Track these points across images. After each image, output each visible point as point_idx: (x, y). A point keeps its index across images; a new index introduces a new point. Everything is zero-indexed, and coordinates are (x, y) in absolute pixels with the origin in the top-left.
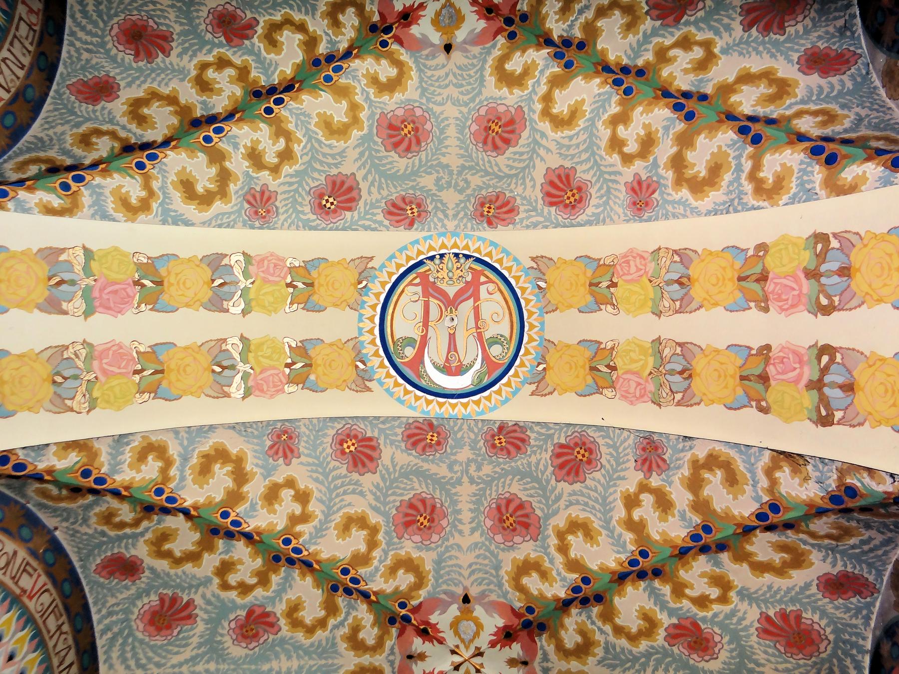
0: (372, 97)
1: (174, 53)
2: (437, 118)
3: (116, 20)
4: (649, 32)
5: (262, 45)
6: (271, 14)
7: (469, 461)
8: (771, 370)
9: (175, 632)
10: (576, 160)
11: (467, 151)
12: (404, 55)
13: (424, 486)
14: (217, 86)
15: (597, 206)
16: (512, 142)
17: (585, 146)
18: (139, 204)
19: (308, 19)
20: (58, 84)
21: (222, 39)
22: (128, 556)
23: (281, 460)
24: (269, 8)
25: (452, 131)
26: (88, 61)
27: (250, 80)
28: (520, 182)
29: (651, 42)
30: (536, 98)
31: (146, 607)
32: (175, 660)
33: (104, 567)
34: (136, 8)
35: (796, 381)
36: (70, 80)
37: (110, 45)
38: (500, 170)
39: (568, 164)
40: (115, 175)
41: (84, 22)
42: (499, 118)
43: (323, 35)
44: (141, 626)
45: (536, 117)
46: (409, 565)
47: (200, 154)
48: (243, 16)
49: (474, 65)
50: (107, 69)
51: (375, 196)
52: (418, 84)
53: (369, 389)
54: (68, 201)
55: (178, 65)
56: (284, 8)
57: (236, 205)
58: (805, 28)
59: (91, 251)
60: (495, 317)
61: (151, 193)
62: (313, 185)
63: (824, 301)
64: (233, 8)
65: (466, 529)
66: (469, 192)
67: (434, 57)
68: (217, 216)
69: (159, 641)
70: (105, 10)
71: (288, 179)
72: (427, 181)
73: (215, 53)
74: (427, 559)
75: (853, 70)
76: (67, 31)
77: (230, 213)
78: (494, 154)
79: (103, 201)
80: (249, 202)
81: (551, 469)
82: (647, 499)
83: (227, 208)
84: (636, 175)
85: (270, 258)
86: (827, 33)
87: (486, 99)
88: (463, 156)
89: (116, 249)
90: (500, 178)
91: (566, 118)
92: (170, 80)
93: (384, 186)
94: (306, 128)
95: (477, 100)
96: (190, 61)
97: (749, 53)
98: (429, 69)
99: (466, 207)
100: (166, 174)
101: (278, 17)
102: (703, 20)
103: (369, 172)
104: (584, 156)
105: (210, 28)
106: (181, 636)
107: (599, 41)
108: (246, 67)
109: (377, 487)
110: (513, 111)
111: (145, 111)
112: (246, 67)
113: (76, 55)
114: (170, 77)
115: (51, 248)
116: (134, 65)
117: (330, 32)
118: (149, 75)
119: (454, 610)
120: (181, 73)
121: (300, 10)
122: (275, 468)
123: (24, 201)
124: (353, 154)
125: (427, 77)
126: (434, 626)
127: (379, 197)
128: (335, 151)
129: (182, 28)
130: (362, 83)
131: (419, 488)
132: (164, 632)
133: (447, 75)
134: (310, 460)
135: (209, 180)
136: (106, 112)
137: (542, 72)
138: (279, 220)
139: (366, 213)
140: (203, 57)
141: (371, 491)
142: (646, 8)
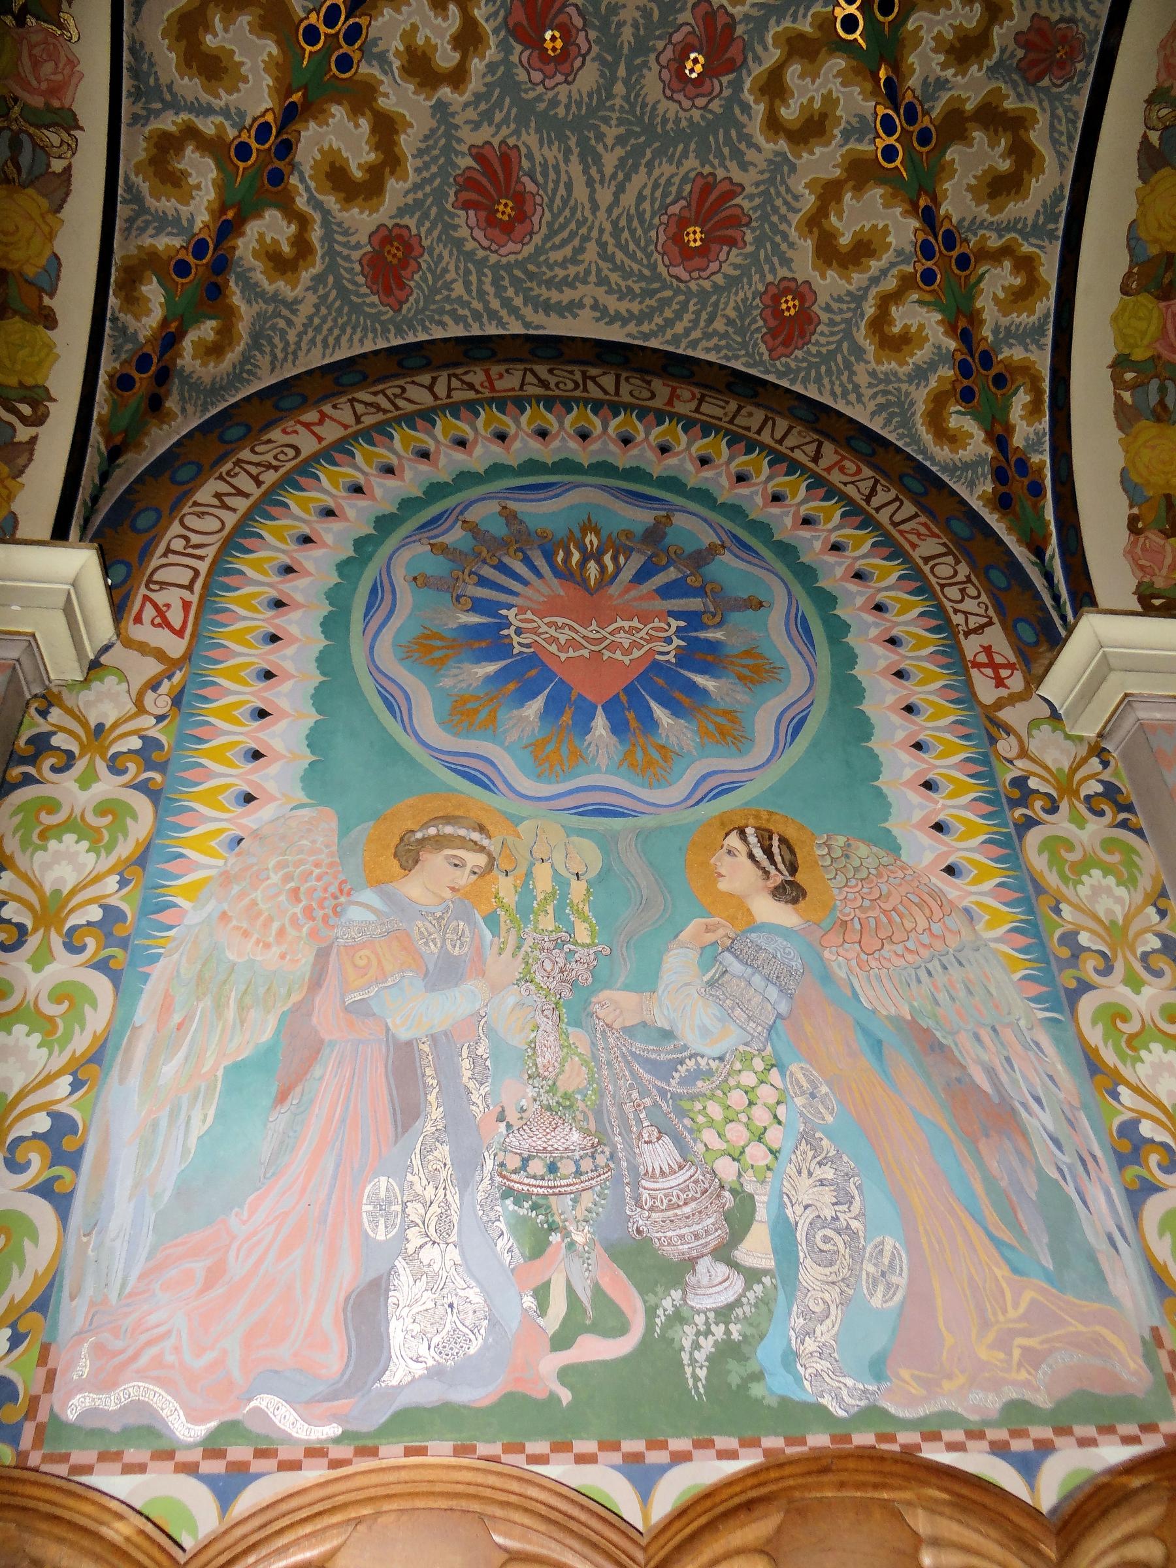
1: (737, 175)
3: (661, 269)
9: (530, 187)
14: (817, 105)
18: (1023, 273)
20: (768, 372)
21: (725, 80)
22: (368, 248)
26: (730, 322)
27: (818, 35)
31: (478, 234)
32: (581, 193)
33: (388, 291)
34: (646, 232)
36: (761, 355)
37: (707, 285)
40: (978, 304)
41: (658, 320)
44: (511, 246)
47: (948, 157)
48: (687, 29)
50: (750, 295)
54: (1020, 380)
55: (762, 172)
57: (1041, 102)
59: (1118, 356)
61: (1006, 251)
64: (670, 47)
69: (541, 220)
73: (750, 99)
76: (670, 348)
77: (1054, 116)
79: (1018, 327)
80: (1040, 77)
83: (1043, 120)
85: (1168, 52)
89: (1115, 319)
92: (788, 190)
96: (759, 150)
100: (978, 221)
105: (701, 102)
106: (540, 179)
108: (789, 41)
111: (845, 240)
112: (789, 41)
113: (715, 340)
114: (782, 189)
115: (1116, 413)
116: (749, 249)
118: (773, 226)
120: (779, 167)
123: (1027, 439)
129: (692, 155)
132: (528, 208)
135: (992, 146)
136: (835, 306)
138: (1083, 20)
140: (755, 126)
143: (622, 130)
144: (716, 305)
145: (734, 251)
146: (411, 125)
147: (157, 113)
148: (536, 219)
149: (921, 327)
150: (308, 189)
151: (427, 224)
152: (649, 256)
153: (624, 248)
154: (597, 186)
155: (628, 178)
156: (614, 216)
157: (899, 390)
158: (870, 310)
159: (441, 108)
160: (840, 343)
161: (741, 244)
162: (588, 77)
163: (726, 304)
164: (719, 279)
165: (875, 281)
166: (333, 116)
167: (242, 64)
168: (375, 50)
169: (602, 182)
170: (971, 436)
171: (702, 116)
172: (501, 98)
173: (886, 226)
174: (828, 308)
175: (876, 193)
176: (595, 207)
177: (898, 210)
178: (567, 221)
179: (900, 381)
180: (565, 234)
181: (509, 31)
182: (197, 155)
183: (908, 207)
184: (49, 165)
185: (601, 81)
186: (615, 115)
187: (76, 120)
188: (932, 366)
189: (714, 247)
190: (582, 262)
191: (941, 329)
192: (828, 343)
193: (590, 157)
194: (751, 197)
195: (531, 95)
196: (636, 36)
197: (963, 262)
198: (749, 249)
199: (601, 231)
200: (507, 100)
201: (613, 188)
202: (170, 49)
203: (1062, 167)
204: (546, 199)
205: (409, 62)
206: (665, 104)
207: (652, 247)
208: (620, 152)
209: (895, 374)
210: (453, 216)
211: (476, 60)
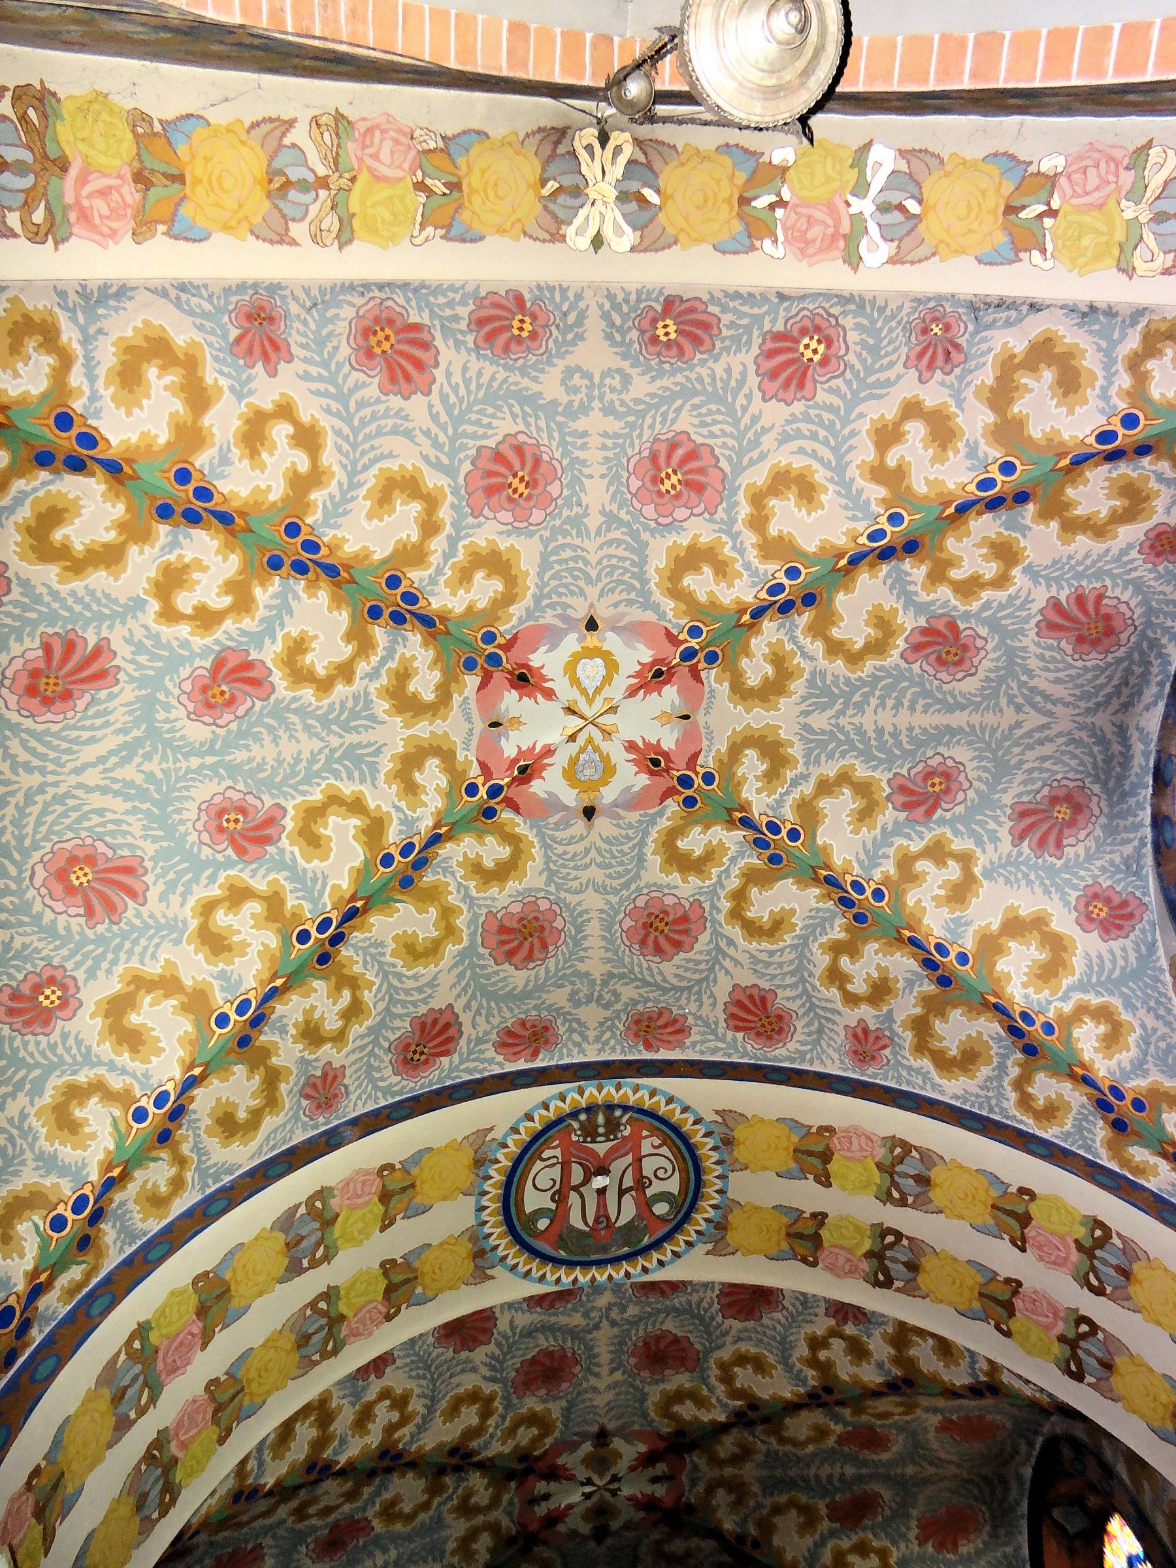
0: (474, 893)
1: (153, 895)
2: (572, 911)
3: (36, 856)
4: (890, 827)
5: (296, 850)
6: (304, 793)
7: (610, 1306)
8: (1018, 1303)
9: (81, 704)
10: (777, 982)
11: (616, 952)
12: (521, 826)
13: (551, 1340)
14: (236, 939)
15: (803, 1043)
16: (686, 946)
17: (792, 967)
19: (365, 790)
23: (373, 1377)
24: (301, 783)
25: (594, 928)
27: (288, 915)
28: (693, 998)
29: (891, 844)
30: (722, 894)
34: (70, 828)
35: (1048, 1328)
37: (38, 907)
38: (665, 980)
39: (765, 985)
42: (666, 913)
43: (393, 811)
45: (721, 918)
46: (532, 1419)
48: (258, 804)
49: (627, 837)
50: (44, 953)
51: (483, 1026)
52: (542, 866)
53: (492, 1277)
55: (164, 916)
56: (325, 778)
58: (1087, 849)
60: (661, 1174)
62: (393, 1038)
63: (1095, 1282)
64: (241, 796)
65: (604, 1371)
66: (618, 1006)
67: (568, 826)
68: (268, 1139)
70: (13, 843)
71: (359, 1043)
72: (559, 997)
73: (221, 879)
74: (556, 1409)
75: (1137, 932)
78: (657, 959)
81: (716, 1306)
82: (837, 1344)
84: (861, 1021)
86: (1112, 862)
87: (647, 886)
88: (610, 961)
90: (665, 991)
91: (766, 927)
92: (157, 946)
93: (495, 1012)
94: (380, 963)
95: (633, 887)
97: (1018, 881)
98: (560, 843)
99: (613, 1026)
101: (317, 796)
102: (961, 819)
103: (473, 997)
104: (789, 980)
105: (205, 837)
106: (91, 712)
107: (819, 831)
108: (276, 893)
109: (493, 1357)
110: (687, 906)
112: (276, 893)
114: (156, 940)
116: (90, 933)
117: (403, 804)
118: (119, 947)
119: (587, 1447)
121: (350, 777)
122: (364, 1389)
124: (447, 980)
125: (559, 856)
126: (564, 1468)
127: (488, 1027)
128: (422, 981)
129: (157, 846)
130: (458, 875)
131: (544, 1342)
132: (59, 704)
133: (587, 851)
134: (408, 1360)
137: (733, 860)
139: (470, 1052)
141: (485, 1364)
142: (888, 790)
143: (159, 775)
144: (22, 924)
145: (82, 920)
146: (116, 580)
147: (74, 320)
148: (49, 716)
149: (93, 1136)
150: (35, 490)
151: (17, 611)
152: (46, 838)
153: (45, 812)
154: (101, 767)
155: (116, 794)
156: (75, 792)
157: (22, 1152)
158: (82, 1078)
159: (138, 604)
160: (37, 1065)
161: (91, 923)
162: (198, 732)
163: (26, 934)
164: (48, 916)
165: (112, 1066)
166: (114, 506)
167: (142, 408)
168: (181, 537)
169: (106, 771)
170: (22, 1256)
171: (193, 844)
172: (158, 658)
173: (163, 1050)
174: (65, 1037)
175: (186, 1026)
176: (78, 771)
177: (181, 1053)
178: (54, 748)
179: (32, 1148)
180: (41, 749)
181: (220, 652)
182: (47, 370)
183: (188, 1061)
184: (10, 209)
185: (197, 745)
186: (171, 765)
187: (63, 241)
188: (64, 1171)
189: (79, 899)
190: (17, 775)
191: (101, 1156)
192: (31, 1055)
193: (127, 752)
194: (138, 915)
195: (169, 685)
196: (242, 763)
197: (406, 883)
198: (90, 933)
199: (56, 784)
200: (160, 664)
201: (102, 783)
202: (135, 329)
203: (252, 1157)
204: (72, 722)
205: (176, 569)
206: (193, 807)
207: (56, 839)
208: (139, 779)
209: (35, 1138)
210: (31, 635)
211: (189, 629)
